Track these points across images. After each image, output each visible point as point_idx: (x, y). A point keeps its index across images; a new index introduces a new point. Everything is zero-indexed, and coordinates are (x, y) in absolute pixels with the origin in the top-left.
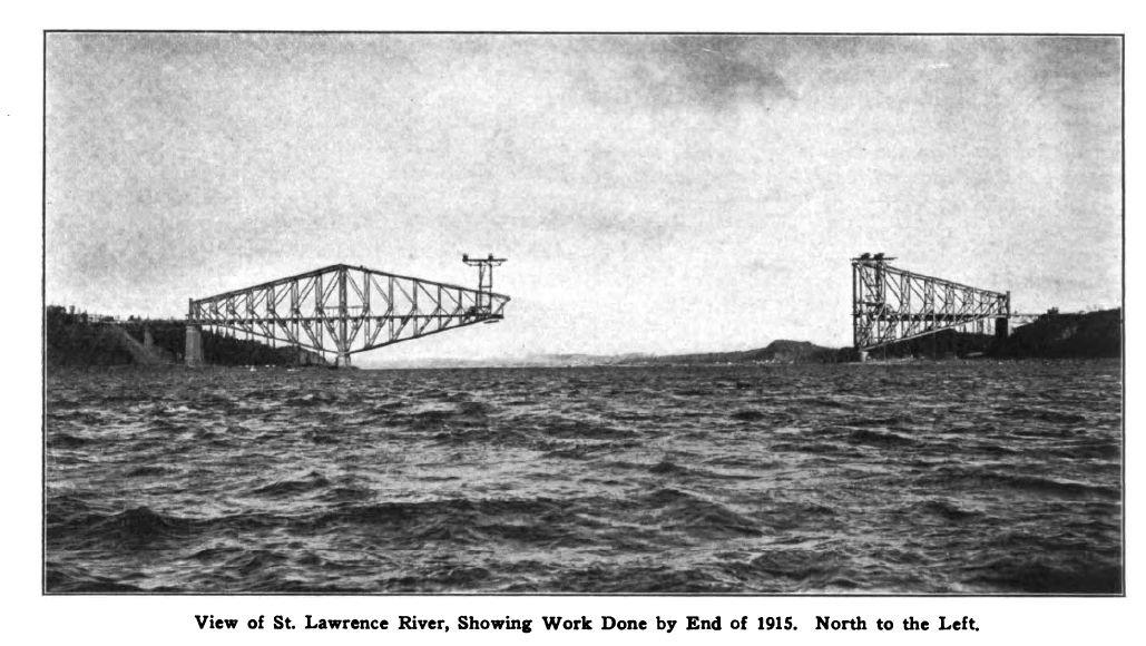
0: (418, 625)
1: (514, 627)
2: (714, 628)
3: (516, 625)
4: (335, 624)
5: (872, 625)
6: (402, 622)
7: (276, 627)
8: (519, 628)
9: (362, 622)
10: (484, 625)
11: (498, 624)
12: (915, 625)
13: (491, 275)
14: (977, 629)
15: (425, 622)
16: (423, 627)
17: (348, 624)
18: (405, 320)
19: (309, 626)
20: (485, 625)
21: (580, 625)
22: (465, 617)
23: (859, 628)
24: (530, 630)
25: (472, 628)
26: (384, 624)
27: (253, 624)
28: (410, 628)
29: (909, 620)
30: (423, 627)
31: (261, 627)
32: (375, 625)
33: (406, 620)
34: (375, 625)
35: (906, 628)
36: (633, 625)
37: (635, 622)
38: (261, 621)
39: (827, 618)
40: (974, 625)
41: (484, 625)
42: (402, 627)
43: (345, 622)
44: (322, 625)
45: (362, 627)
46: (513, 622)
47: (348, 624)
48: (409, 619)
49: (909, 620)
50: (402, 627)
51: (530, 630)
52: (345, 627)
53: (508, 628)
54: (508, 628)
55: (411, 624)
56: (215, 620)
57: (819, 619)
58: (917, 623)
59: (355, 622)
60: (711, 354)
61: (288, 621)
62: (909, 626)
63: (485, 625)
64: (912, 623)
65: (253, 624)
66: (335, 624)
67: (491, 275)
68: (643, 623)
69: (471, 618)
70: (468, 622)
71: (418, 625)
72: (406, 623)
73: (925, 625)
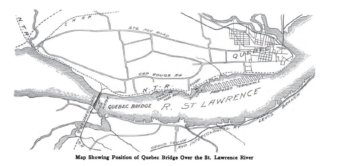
0: (246, 158)
1: (104, 159)
2: (170, 159)
3: (105, 158)
4: (223, 158)
5: (133, 158)
6: (241, 157)
7: (205, 159)
8: (106, 159)
9: (230, 157)
10: (96, 158)
11: (100, 158)
12: (93, 158)
13: (72, 62)
14: (210, 159)
15: (248, 157)
16: (247, 159)
17: (226, 158)
18: (237, 37)
19: (215, 159)
20: (96, 158)
21: (167, 158)
22: (90, 156)
23: (197, 159)
24: (109, 159)
25: (92, 159)
26: (236, 158)
27: (135, 158)
28: (243, 159)
29: (196, 157)
30: (247, 159)
31: (138, 159)
32: (234, 158)
33: (242, 157)
34: (234, 158)
35: (196, 159)
36: (130, 158)
37: (232, 157)
38: (138, 157)
39: (79, 156)
40: (209, 158)
41: (96, 158)
42: (241, 159)
43: (226, 157)
44: (219, 158)
45: (230, 159)
46: (104, 157)
47: (226, 158)
48: (243, 157)
49: (196, 157)
50: (241, 159)
51: (109, 159)
52: (226, 159)
53: (102, 159)
54: (102, 159)
55: (244, 158)
56: (126, 157)
57: (76, 156)
58: (199, 157)
59: (228, 157)
60: (295, 66)
61: (209, 157)
62: (196, 158)
63: (96, 158)
64: (197, 157)
65: (135, 158)
66: (223, 158)
67: (72, 62)
68: (236, 157)
69: (92, 156)
70: (91, 157)
71: (246, 158)
72: (242, 158)
73: (201, 158)
